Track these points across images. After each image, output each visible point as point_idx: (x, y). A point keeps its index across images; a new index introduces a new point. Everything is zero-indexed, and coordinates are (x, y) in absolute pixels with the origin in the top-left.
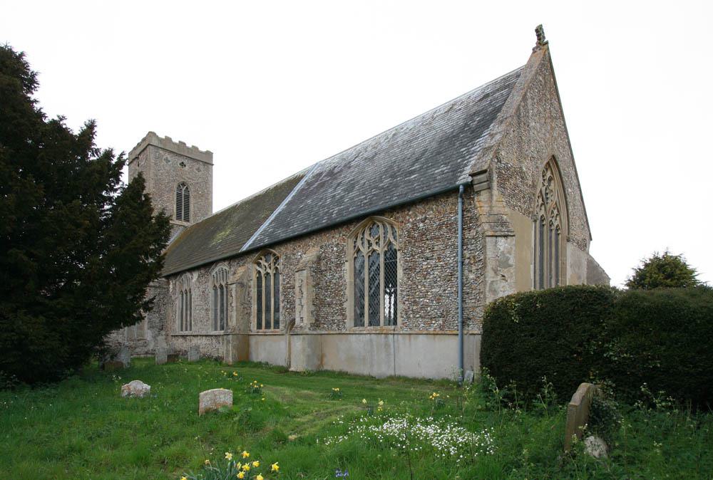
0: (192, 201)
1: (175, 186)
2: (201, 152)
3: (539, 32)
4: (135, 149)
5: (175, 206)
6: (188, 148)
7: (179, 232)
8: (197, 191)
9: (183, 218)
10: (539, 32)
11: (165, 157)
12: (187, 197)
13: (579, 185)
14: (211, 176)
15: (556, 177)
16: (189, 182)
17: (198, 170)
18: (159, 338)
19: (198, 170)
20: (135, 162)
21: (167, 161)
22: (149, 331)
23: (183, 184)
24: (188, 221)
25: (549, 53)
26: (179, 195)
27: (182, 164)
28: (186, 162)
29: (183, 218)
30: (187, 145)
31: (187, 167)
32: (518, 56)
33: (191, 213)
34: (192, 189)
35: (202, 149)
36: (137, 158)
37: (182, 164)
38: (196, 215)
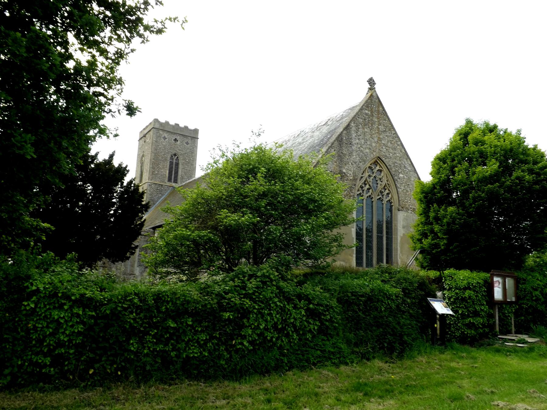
0: (181, 166)
1: (169, 156)
2: (191, 130)
3: (371, 82)
4: (144, 129)
5: (168, 172)
6: (181, 128)
7: (169, 191)
8: (185, 159)
9: (173, 181)
10: (371, 82)
11: (163, 136)
12: (177, 164)
13: (415, 170)
14: (196, 147)
15: (385, 170)
16: (179, 152)
17: (187, 143)
18: (145, 274)
19: (187, 143)
20: (143, 139)
21: (165, 138)
22: (138, 268)
23: (175, 155)
24: (176, 182)
25: (377, 94)
26: (171, 163)
27: (176, 140)
28: (178, 138)
29: (173, 181)
30: (180, 125)
31: (179, 142)
32: (359, 96)
33: (179, 176)
34: (181, 158)
35: (191, 127)
36: (145, 136)
37: (176, 140)
38: (182, 178)
